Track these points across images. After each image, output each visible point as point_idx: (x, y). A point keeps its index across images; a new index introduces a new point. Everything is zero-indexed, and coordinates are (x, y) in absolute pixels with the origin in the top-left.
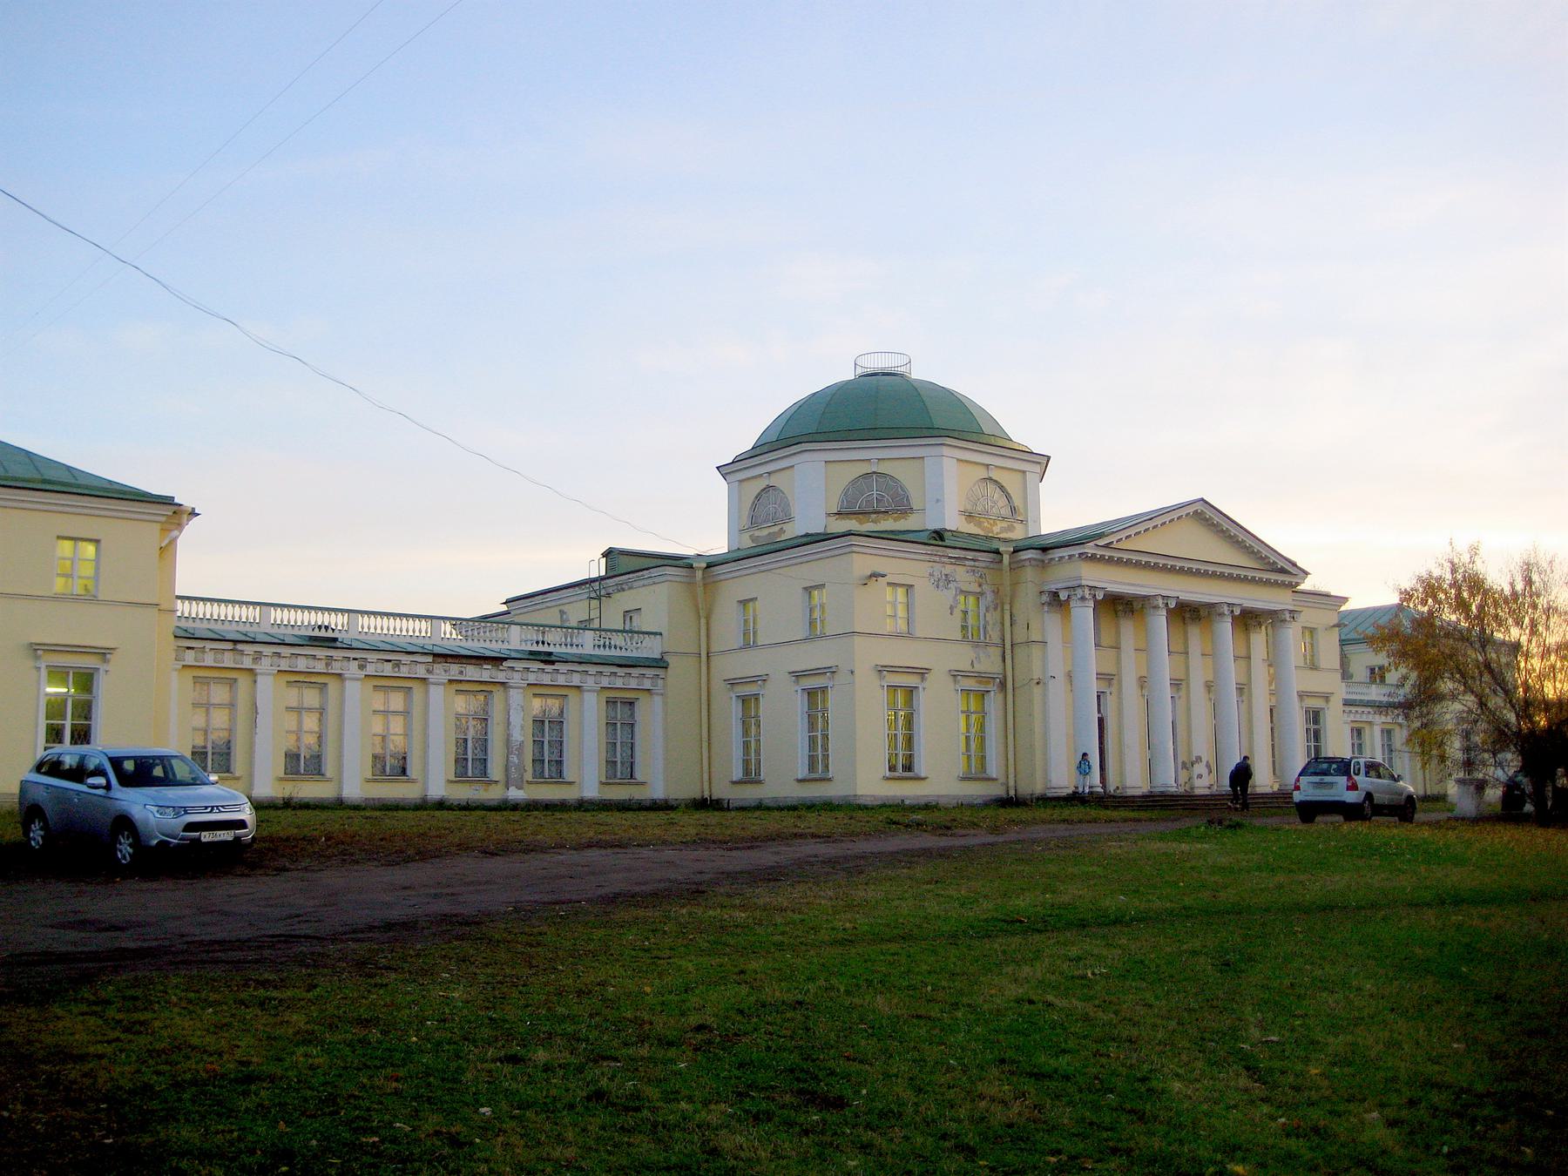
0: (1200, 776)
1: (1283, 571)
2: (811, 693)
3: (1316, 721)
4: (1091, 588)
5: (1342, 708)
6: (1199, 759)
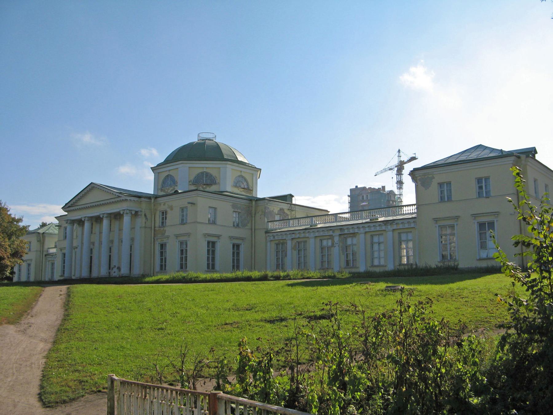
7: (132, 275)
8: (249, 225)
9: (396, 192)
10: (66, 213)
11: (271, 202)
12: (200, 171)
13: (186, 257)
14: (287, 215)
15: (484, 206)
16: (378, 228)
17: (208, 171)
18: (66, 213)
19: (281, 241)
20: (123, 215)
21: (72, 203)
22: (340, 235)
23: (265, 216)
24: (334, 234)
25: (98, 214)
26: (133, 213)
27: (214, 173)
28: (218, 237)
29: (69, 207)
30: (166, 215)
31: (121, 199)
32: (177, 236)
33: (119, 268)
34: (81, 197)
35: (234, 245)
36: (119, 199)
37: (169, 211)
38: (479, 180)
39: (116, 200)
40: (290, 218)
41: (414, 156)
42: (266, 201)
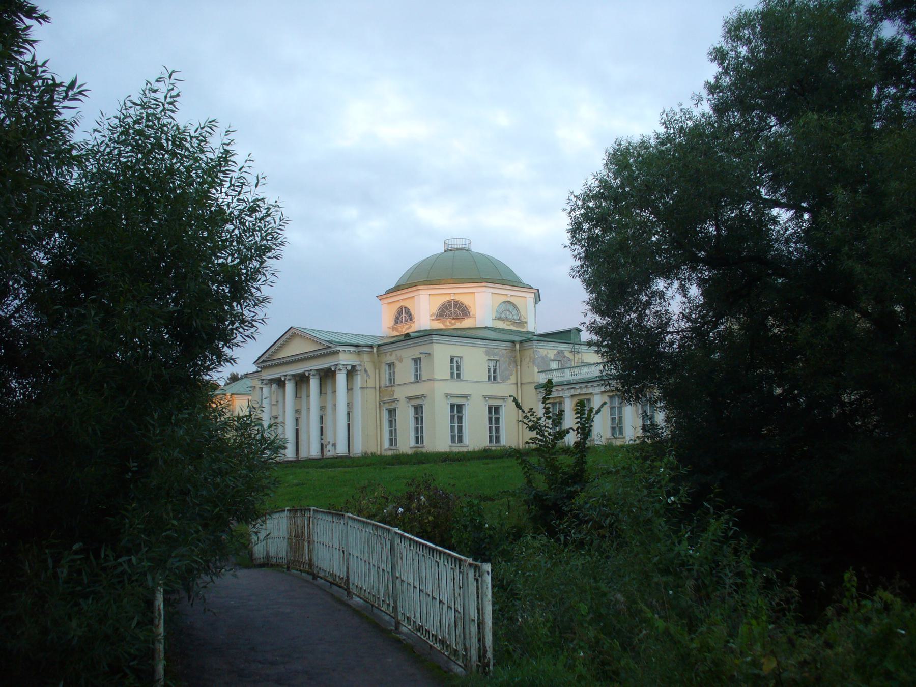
7: (351, 455)
8: (513, 379)
11: (543, 344)
12: (448, 298)
13: (422, 427)
15: (456, 388)
17: (458, 298)
20: (334, 372)
21: (267, 355)
25: (302, 371)
26: (349, 368)
27: (466, 300)
29: (264, 361)
32: (410, 399)
33: (334, 445)
35: (490, 408)
36: (328, 350)
37: (397, 363)
39: (325, 351)
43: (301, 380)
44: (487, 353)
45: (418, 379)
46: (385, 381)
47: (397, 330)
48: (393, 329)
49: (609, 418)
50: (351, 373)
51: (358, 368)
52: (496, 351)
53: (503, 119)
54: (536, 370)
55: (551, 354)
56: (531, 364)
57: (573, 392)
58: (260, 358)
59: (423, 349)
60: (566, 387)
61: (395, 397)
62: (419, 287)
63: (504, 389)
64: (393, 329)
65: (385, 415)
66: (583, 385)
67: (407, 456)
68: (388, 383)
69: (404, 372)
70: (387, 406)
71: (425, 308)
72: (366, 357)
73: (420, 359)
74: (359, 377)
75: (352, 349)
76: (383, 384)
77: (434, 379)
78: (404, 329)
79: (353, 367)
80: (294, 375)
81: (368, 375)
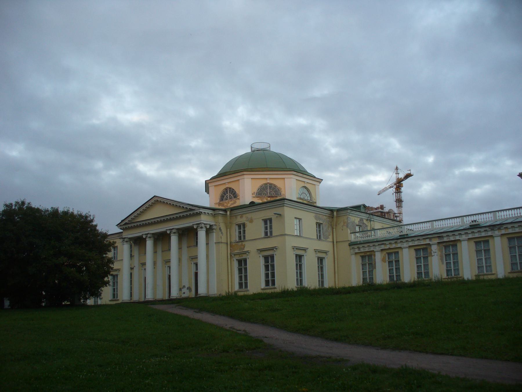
0: (184, 293)
1: (191, 210)
2: (266, 258)
3: (300, 261)
4: (204, 224)
5: (348, 248)
6: (184, 287)
9: (396, 210)
10: (122, 231)
11: (353, 212)
12: (264, 182)
14: (366, 226)
16: (483, 234)
18: (122, 231)
19: (368, 254)
21: (129, 219)
22: (439, 243)
23: (347, 227)
24: (375, 250)
26: (208, 227)
28: (305, 250)
29: (126, 224)
30: (244, 227)
31: (195, 212)
34: (145, 211)
36: (191, 212)
37: (248, 224)
38: (265, 221)
40: (369, 229)
41: (409, 172)
42: (349, 211)
43: (162, 238)
44: (316, 218)
45: (268, 234)
46: (235, 237)
47: (223, 205)
48: (219, 204)
49: (416, 265)
50: (209, 230)
51: (214, 227)
52: (321, 216)
53: (192, 112)
54: (349, 232)
55: (357, 221)
56: (345, 227)
57: (383, 247)
58: (122, 221)
59: (278, 211)
60: (376, 244)
61: (246, 250)
62: (245, 173)
63: (325, 246)
64: (219, 204)
65: (236, 265)
66: (393, 242)
67: (224, 296)
68: (237, 239)
69: (255, 229)
70: (237, 257)
71: (248, 189)
72: (220, 219)
73: (270, 220)
74: (214, 234)
75: (210, 212)
76: (233, 240)
77: (285, 235)
78: (230, 204)
79: (211, 226)
80: (153, 234)
81: (222, 233)
